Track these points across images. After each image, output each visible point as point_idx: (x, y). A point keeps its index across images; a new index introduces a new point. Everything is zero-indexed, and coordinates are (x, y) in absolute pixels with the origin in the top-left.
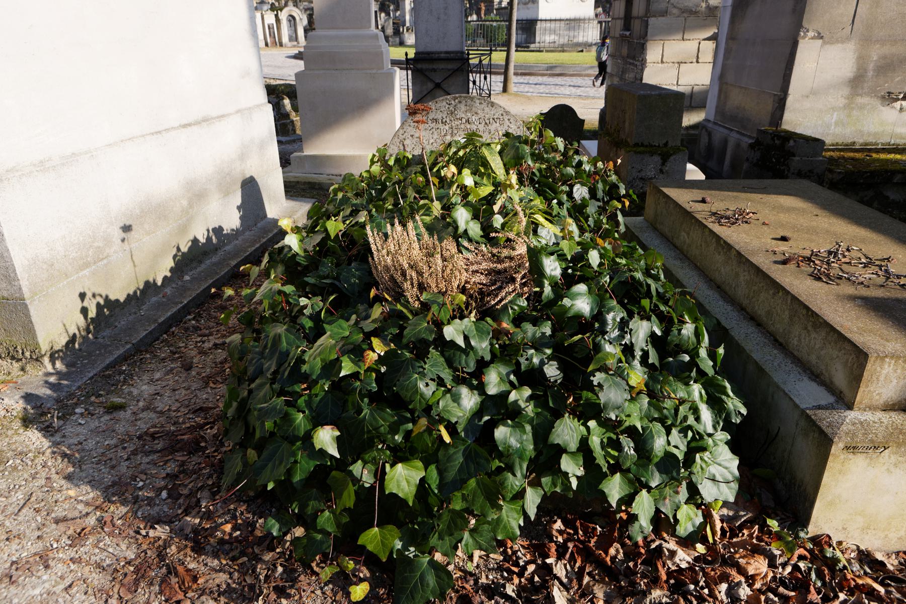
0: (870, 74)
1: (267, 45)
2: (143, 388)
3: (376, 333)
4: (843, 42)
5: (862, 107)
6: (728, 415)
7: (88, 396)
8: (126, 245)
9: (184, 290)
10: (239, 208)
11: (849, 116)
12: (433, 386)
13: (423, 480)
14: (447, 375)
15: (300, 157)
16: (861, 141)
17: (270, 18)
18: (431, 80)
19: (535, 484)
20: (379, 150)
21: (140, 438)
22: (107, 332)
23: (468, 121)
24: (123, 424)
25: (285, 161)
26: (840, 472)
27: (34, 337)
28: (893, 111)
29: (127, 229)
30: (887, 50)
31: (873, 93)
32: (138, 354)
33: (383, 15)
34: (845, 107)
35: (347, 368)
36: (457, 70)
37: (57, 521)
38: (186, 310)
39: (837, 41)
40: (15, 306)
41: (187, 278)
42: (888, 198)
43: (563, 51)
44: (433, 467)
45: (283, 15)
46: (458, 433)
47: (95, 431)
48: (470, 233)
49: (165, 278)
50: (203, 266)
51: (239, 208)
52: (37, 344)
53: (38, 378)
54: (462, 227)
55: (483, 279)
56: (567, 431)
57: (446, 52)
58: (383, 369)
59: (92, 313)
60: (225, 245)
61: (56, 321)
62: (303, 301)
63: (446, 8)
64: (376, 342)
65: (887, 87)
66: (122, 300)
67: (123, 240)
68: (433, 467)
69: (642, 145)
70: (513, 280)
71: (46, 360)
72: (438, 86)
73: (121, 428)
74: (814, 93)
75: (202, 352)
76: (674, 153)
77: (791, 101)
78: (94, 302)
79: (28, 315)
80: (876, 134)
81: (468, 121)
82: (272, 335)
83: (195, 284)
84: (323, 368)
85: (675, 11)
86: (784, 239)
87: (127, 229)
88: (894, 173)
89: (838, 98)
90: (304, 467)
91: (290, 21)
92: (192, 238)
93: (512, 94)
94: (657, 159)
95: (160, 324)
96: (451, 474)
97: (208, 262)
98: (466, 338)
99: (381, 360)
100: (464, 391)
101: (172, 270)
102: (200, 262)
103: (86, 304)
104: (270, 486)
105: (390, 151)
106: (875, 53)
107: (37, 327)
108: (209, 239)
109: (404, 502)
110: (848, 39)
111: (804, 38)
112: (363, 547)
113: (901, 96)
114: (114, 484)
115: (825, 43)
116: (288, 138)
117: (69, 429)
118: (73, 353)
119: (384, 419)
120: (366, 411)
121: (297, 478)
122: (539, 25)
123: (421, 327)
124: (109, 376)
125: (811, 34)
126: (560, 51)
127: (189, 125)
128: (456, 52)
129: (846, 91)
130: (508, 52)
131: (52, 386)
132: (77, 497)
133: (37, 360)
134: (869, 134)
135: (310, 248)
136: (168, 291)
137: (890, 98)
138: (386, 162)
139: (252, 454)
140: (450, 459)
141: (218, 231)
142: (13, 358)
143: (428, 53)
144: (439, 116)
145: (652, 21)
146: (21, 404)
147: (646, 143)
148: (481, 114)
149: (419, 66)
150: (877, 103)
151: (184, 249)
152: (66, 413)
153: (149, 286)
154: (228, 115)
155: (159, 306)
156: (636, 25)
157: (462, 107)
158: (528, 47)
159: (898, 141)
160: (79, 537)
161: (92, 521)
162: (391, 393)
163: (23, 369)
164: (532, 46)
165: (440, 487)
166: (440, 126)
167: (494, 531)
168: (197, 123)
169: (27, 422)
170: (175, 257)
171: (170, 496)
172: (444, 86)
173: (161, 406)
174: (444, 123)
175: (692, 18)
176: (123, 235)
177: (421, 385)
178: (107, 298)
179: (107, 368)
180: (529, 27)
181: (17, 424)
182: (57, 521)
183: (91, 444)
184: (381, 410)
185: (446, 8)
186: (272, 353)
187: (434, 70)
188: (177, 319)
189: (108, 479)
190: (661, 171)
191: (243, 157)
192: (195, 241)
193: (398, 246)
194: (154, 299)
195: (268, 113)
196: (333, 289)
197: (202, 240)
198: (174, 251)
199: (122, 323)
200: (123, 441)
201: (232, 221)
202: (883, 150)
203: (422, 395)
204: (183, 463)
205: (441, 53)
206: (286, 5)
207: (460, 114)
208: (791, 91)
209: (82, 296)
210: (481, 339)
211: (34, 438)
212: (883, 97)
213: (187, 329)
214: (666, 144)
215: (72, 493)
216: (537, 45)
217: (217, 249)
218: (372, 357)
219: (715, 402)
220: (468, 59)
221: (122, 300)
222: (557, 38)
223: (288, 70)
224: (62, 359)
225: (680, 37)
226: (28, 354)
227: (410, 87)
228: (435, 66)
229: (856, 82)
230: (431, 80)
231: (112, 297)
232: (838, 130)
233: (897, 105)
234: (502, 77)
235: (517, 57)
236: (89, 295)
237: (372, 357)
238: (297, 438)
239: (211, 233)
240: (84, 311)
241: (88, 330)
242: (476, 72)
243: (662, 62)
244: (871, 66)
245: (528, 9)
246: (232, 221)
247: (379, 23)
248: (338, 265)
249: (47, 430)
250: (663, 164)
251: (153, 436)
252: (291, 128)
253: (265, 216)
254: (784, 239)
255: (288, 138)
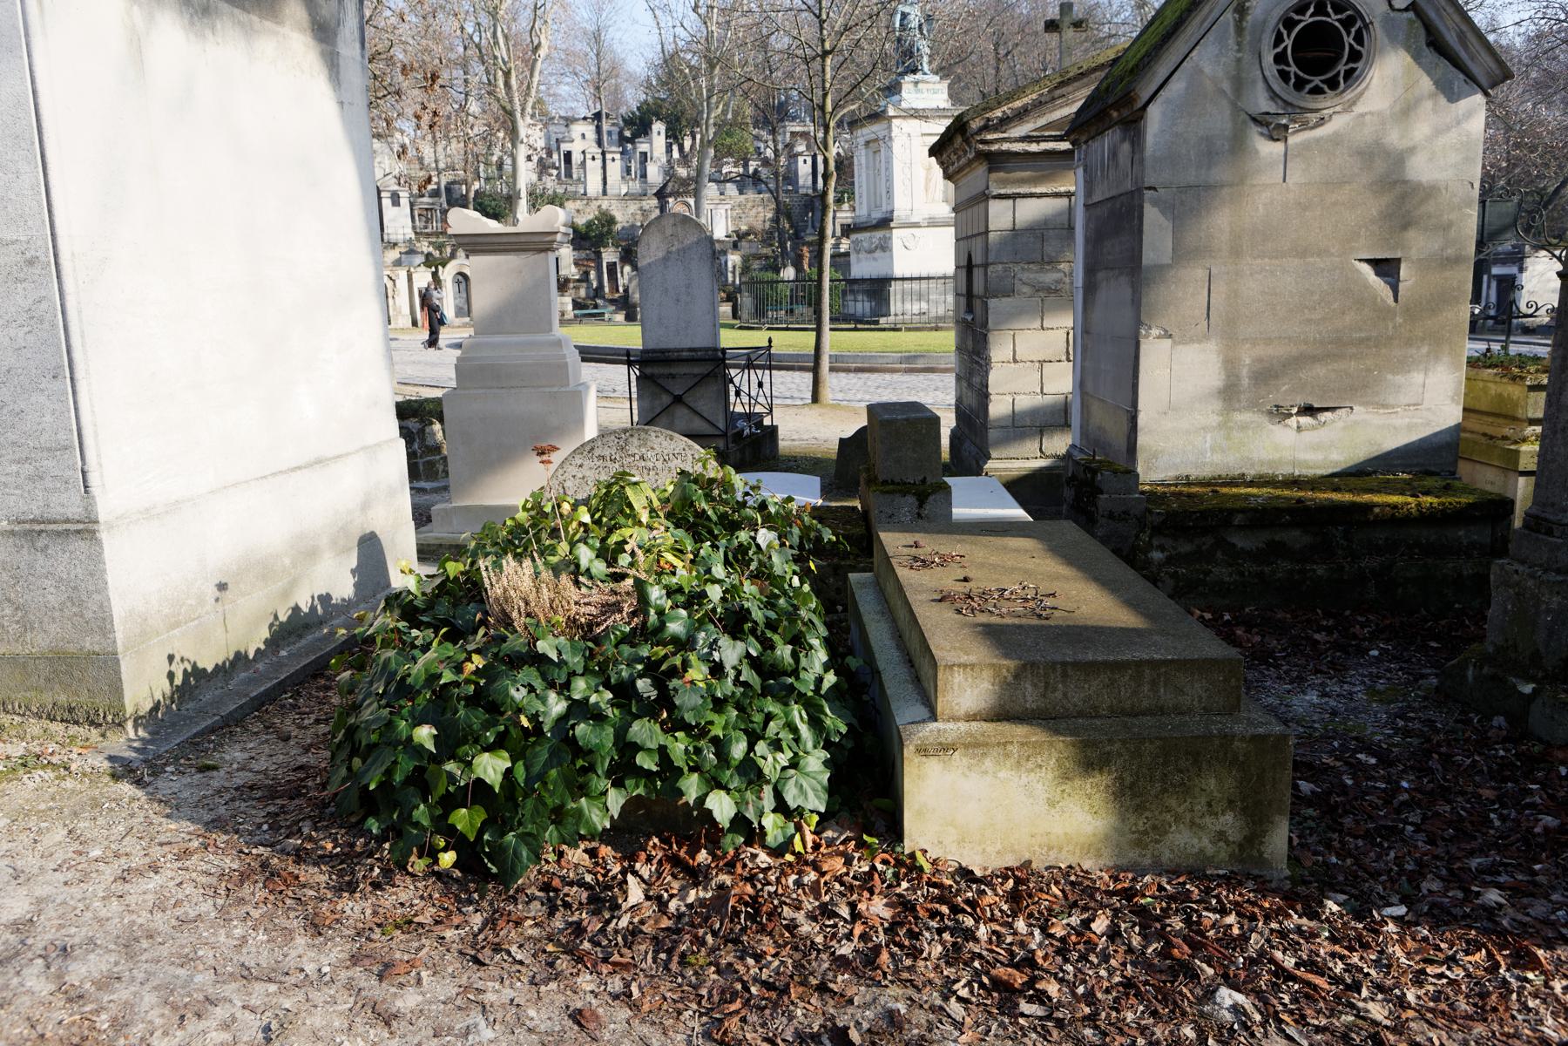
0: (1245, 382)
1: (415, 323)
2: (234, 754)
3: (478, 651)
4: (1200, 342)
5: (1244, 427)
6: (828, 735)
7: (177, 759)
8: (219, 607)
9: (280, 665)
10: (353, 572)
11: (1228, 438)
12: (524, 691)
13: (509, 772)
14: (538, 684)
15: (445, 510)
16: (1253, 472)
17: (423, 278)
18: (667, 391)
19: (618, 784)
20: (533, 495)
21: (237, 789)
22: (191, 705)
23: (642, 458)
24: (218, 779)
25: (422, 517)
26: (919, 777)
27: (121, 697)
28: (1288, 430)
29: (222, 587)
30: (1261, 351)
31: (1254, 405)
32: (229, 726)
33: (627, 269)
34: (1220, 426)
35: (447, 677)
36: (708, 375)
37: (161, 844)
38: (281, 687)
39: (1192, 341)
40: (105, 662)
41: (283, 653)
42: (1234, 545)
43: (937, 329)
44: (520, 763)
45: (448, 274)
46: (543, 733)
47: (190, 785)
48: (594, 571)
49: (258, 650)
50: (303, 642)
51: (353, 572)
52: (123, 705)
53: (125, 741)
54: (584, 563)
55: (594, 611)
56: (644, 731)
57: (691, 350)
58: (482, 682)
59: (178, 681)
60: (332, 618)
61: (144, 684)
62: (415, 632)
63: (688, 286)
64: (475, 657)
65: (1273, 398)
66: (210, 670)
67: (217, 600)
68: (520, 763)
69: (893, 483)
70: (620, 611)
71: (129, 725)
72: (678, 400)
73: (216, 784)
74: (1171, 408)
75: (300, 727)
76: (933, 492)
77: (1142, 420)
78: (182, 667)
79: (118, 672)
80: (1270, 463)
81: (642, 458)
82: (382, 658)
83: (293, 659)
84: (427, 680)
85: (1026, 289)
86: (966, 580)
87: (222, 587)
88: (1232, 512)
89: (1209, 415)
90: (406, 766)
91: (459, 282)
92: (292, 605)
93: (826, 406)
94: (911, 499)
95: (252, 699)
96: (536, 769)
97: (310, 637)
98: (560, 653)
99: (477, 672)
100: (552, 696)
101: (266, 642)
102: (300, 637)
103: (173, 668)
104: (372, 787)
105: (547, 495)
106: (1247, 357)
107: (125, 686)
108: (313, 608)
109: (491, 788)
110: (1206, 337)
111: (1147, 336)
112: (453, 827)
113: (1295, 410)
114: (213, 821)
115: (1175, 343)
116: (435, 485)
117: (160, 784)
118: (154, 720)
119: (477, 718)
120: (462, 713)
121: (398, 778)
122: (895, 288)
123: (516, 643)
124: (197, 744)
125: (1155, 332)
126: (931, 329)
127: (299, 468)
128: (706, 349)
129: (1217, 405)
130: (819, 331)
131: (136, 750)
132: (180, 829)
133: (120, 725)
134: (1262, 463)
135: (429, 590)
136: (260, 666)
137: (1280, 414)
138: (541, 508)
139: (357, 762)
140: (536, 755)
141: (325, 599)
142: (92, 723)
143: (663, 351)
144: (607, 452)
145: (992, 303)
146: (106, 764)
147: (897, 480)
148: (659, 450)
149: (648, 371)
150: (1264, 419)
151: (283, 618)
152: (156, 772)
153: (240, 659)
154: (348, 454)
155: (250, 681)
156: (977, 304)
157: (635, 441)
158: (877, 322)
159: (1305, 472)
160: (187, 853)
161: (195, 844)
162: (487, 701)
163: (103, 735)
164: (882, 320)
165: (527, 781)
166: (609, 463)
167: (577, 824)
168: (309, 465)
169: (115, 777)
170: (271, 625)
171: (270, 828)
172: (688, 399)
173: (255, 766)
174: (614, 461)
175: (1052, 298)
176: (218, 594)
177: (513, 692)
178: (194, 666)
179: (195, 735)
180: (878, 288)
181: (107, 779)
182: (161, 844)
183: (186, 794)
184: (475, 712)
185: (688, 286)
186: (382, 674)
187: (673, 376)
188: (270, 697)
189: (207, 817)
190: (919, 515)
191: (365, 506)
192: (296, 609)
193: (513, 580)
194: (243, 675)
195: (397, 453)
196: (445, 623)
197: (305, 609)
198: (271, 619)
199: (208, 697)
200: (219, 791)
201: (343, 588)
202: (1251, 484)
203: (512, 699)
204: (283, 806)
205: (682, 350)
206: (453, 256)
207: (632, 450)
208: (1140, 406)
209: (171, 658)
210: (574, 655)
211: (126, 788)
212: (1270, 413)
213: (283, 707)
214: (924, 481)
215: (173, 827)
216: (891, 319)
217: (321, 622)
218: (470, 667)
219: (815, 723)
220: (724, 359)
221: (210, 670)
222: (924, 305)
223: (436, 373)
224: (145, 728)
225: (1037, 324)
226: (109, 718)
227: (634, 396)
228: (673, 371)
229: (1229, 393)
230: (667, 391)
231: (200, 665)
232: (1217, 458)
233: (1293, 421)
234: (809, 376)
235: (837, 341)
236: (177, 658)
237: (470, 667)
238: (399, 742)
239: (316, 601)
240: (171, 676)
241: (172, 698)
242: (762, 367)
243: (1015, 361)
244: (1245, 372)
245: (875, 259)
246: (343, 588)
247: (620, 282)
248: (455, 605)
249: (139, 783)
250: (921, 506)
251: (251, 788)
252: (441, 468)
253: (389, 585)
254: (966, 580)
255: (435, 485)
